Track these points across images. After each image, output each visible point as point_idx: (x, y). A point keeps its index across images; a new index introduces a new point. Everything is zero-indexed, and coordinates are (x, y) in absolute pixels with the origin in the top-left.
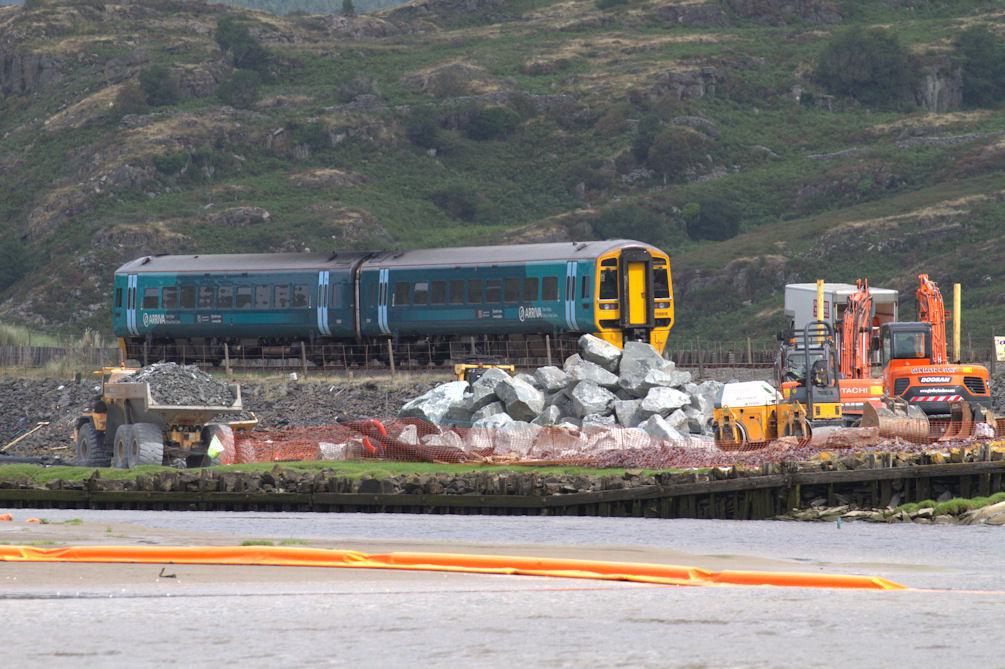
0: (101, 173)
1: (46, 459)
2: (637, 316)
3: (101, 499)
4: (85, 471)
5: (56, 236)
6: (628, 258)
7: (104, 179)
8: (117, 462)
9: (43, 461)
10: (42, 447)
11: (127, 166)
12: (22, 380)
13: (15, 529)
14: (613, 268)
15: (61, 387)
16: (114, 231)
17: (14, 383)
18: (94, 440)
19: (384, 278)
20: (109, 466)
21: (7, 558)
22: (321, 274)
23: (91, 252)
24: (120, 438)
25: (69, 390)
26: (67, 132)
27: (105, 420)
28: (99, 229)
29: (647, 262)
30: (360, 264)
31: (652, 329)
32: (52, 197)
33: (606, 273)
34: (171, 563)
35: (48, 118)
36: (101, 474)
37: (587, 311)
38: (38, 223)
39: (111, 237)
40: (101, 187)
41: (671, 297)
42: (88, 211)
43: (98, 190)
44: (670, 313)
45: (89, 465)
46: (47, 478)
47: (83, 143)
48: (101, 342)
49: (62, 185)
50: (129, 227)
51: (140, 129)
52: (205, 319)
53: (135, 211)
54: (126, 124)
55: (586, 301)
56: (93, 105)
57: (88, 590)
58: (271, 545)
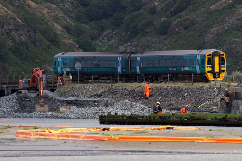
0: (227, 23)
1: (211, 111)
2: (217, 70)
3: (228, 123)
4: (222, 115)
5: (213, 43)
6: (214, 54)
7: (228, 25)
8: (232, 112)
9: (210, 111)
10: (209, 107)
11: (236, 21)
12: (203, 87)
13: (202, 132)
14: (210, 57)
15: (215, 89)
16: (232, 41)
17: (201, 88)
18: (226, 105)
19: (138, 59)
20: (230, 113)
21: (200, 141)
22: (119, 58)
23: (224, 47)
24: (233, 104)
25: (218, 90)
26: (217, 10)
27: (229, 99)
28: (226, 40)
29: (219, 55)
30: (130, 55)
31: (221, 73)
32: (212, 31)
33: (209, 58)
34: (238, 143)
35: (211, 6)
36: (228, 116)
37: (203, 68)
38: (208, 39)
39: (230, 43)
40: (227, 27)
41: (225, 65)
42: (223, 35)
43: (227, 28)
44: (225, 69)
45: (224, 113)
46: (211, 117)
47: (222, 14)
48: (227, 75)
49: (215, 27)
50: (236, 39)
51: (240, 9)
52: (171, 69)
53: (238, 34)
54: (235, 8)
55: (203, 65)
56: (225, 2)
57: (224, 151)
58: (123, 135)
